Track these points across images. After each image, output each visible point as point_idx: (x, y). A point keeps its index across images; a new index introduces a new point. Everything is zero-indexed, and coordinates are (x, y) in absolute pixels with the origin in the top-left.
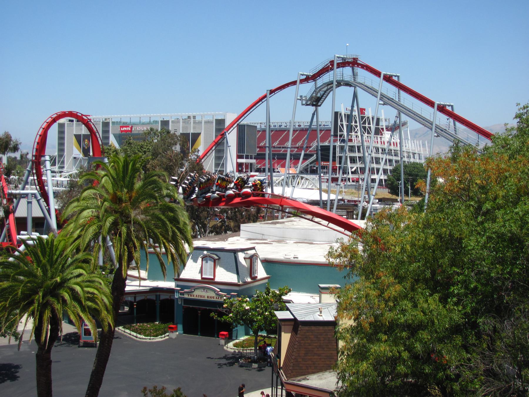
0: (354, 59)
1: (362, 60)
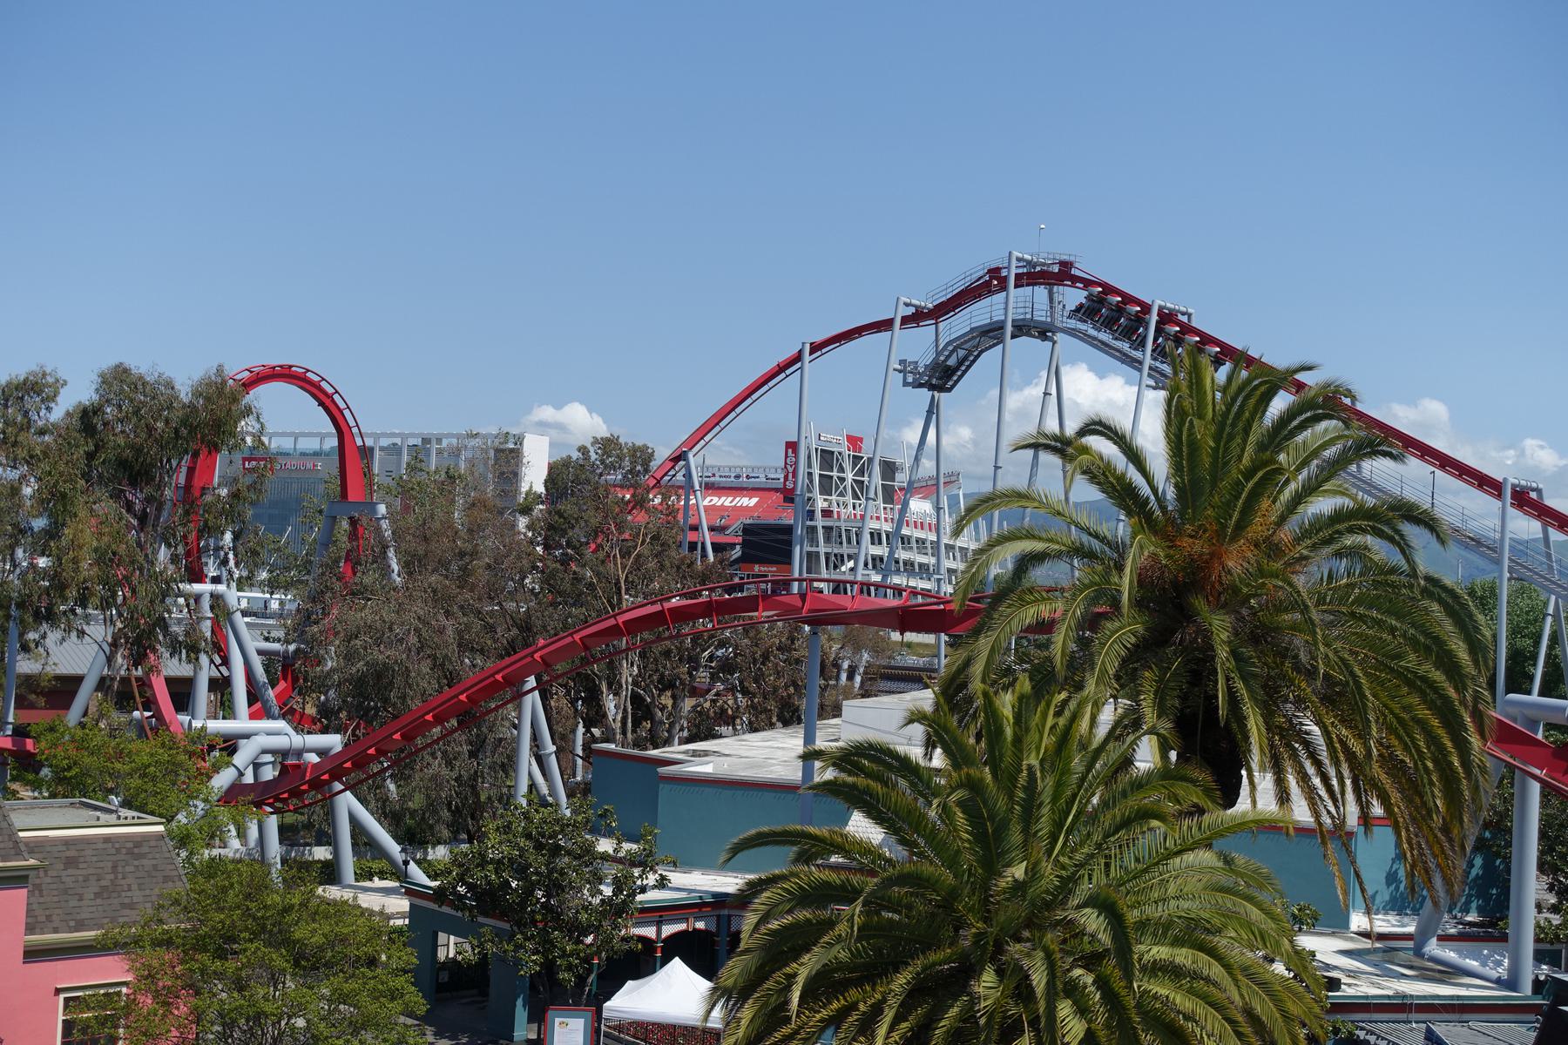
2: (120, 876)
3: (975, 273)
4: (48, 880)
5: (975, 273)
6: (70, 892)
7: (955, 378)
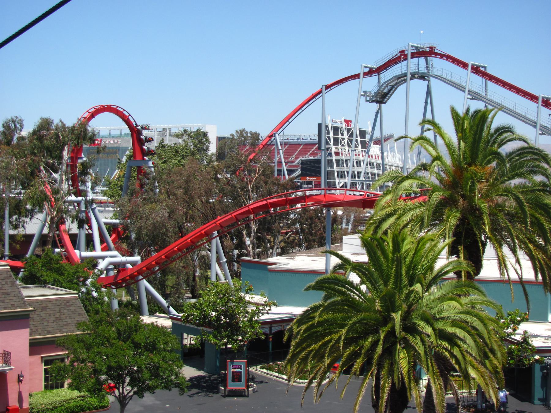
1: (440, 49)
4: (36, 316)
6: (44, 320)
7: (387, 98)
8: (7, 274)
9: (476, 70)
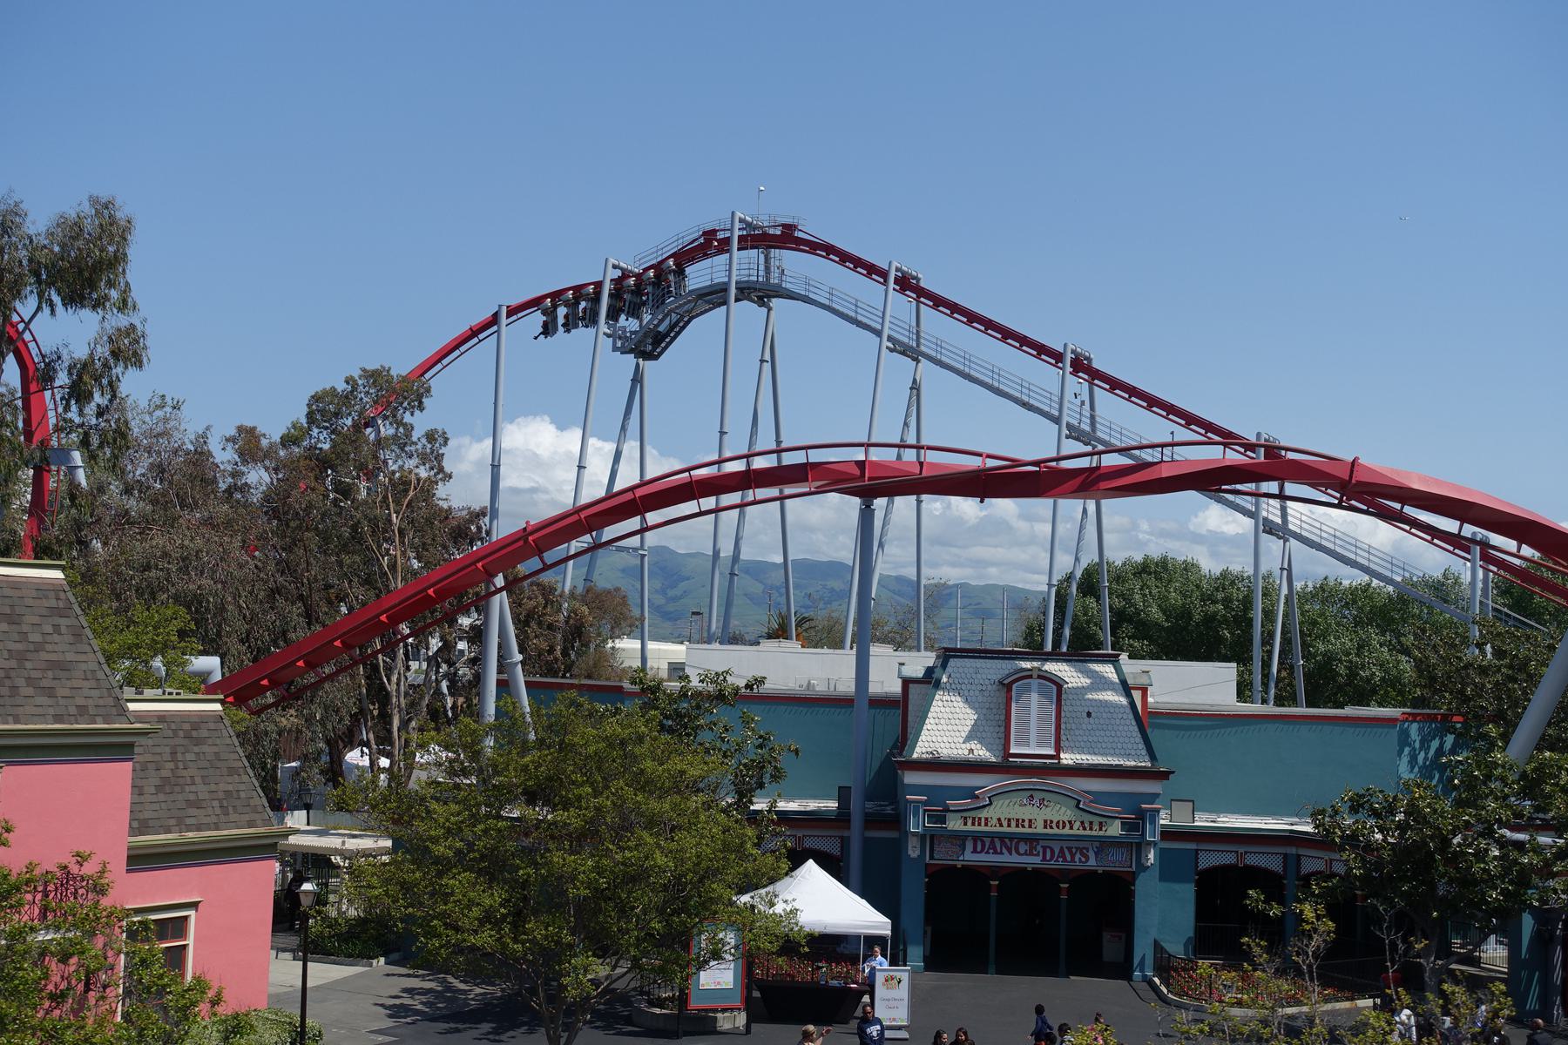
0: (784, 226)
1: (810, 228)
2: (181, 765)
3: (688, 235)
5: (688, 235)
7: (663, 345)
8: (58, 599)
9: (906, 283)
